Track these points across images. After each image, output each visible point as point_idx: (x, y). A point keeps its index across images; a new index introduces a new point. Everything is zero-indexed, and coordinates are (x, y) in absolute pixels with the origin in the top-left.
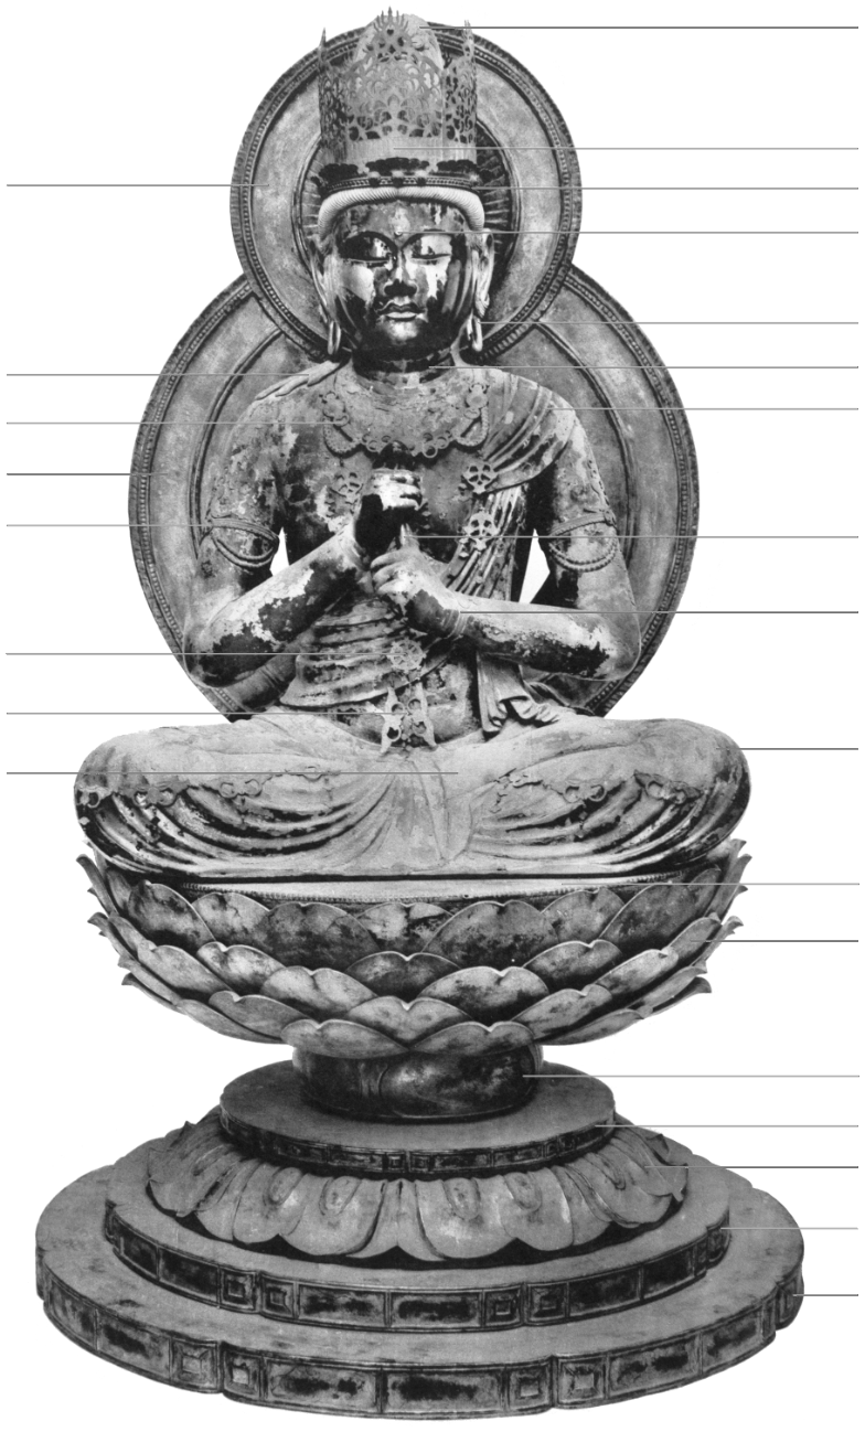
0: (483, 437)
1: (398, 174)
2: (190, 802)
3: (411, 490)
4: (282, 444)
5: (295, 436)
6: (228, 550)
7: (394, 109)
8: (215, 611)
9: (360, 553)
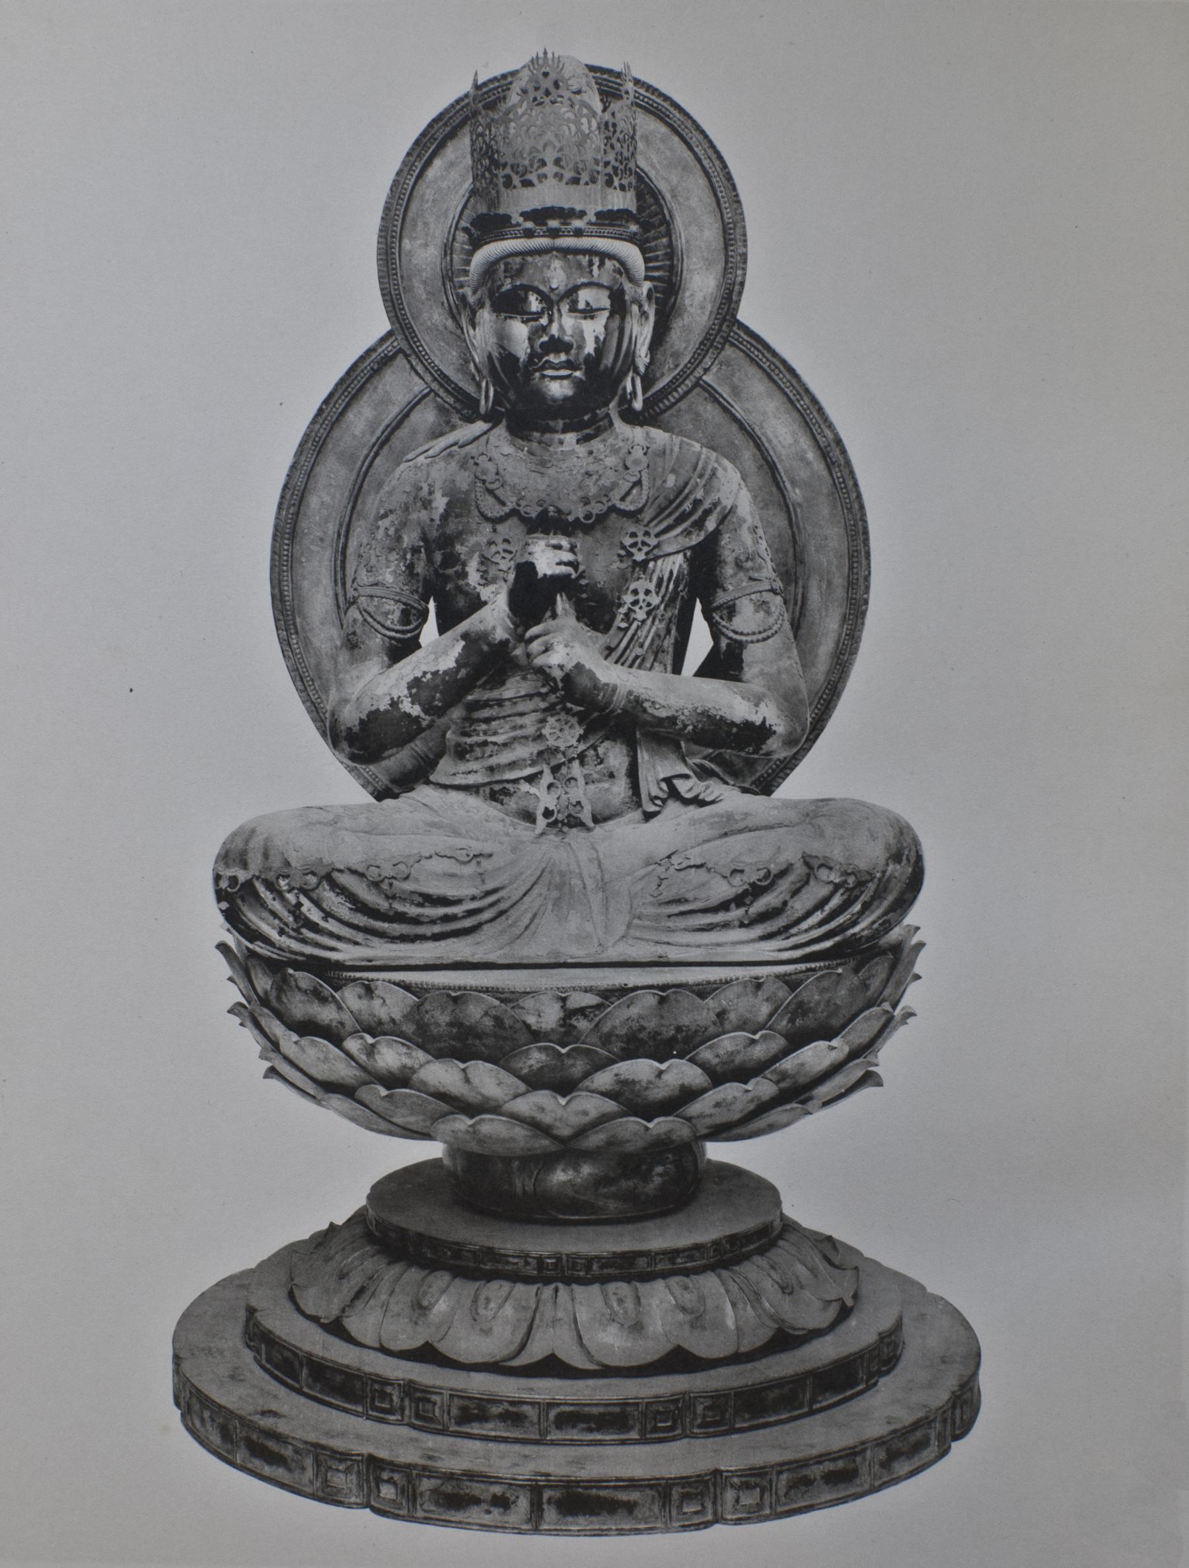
1: (553, 223)
2: (335, 886)
3: (567, 556)
5: (445, 500)
7: (550, 156)
8: (360, 685)
9: (514, 623)
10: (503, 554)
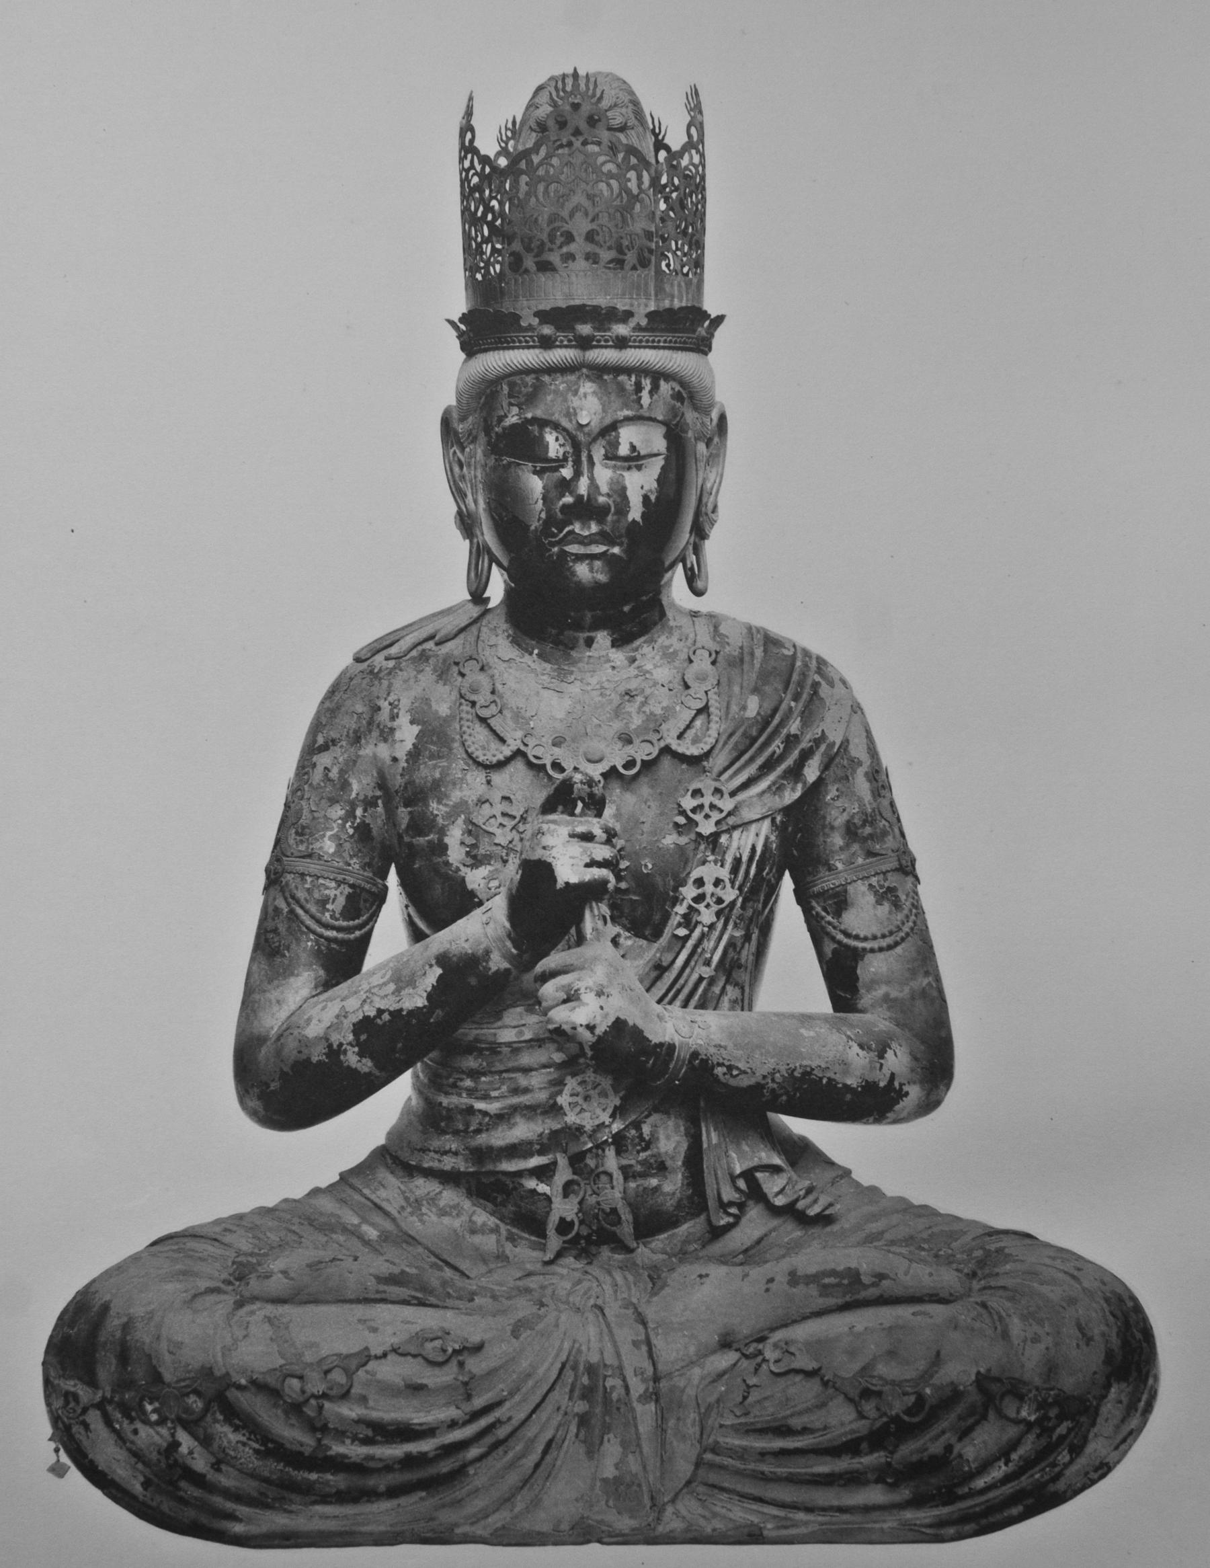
0: (712, 740)
1: (585, 329)
2: (233, 1415)
3: (602, 852)
4: (394, 741)
5: (416, 729)
6: (306, 911)
7: (581, 226)
8: (283, 1014)
10: (500, 820)
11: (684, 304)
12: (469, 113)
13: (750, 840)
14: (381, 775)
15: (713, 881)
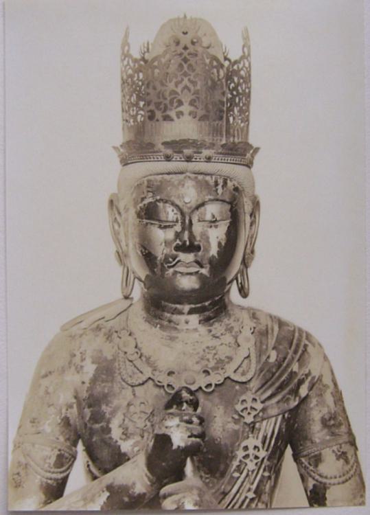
0: (253, 373)
1: (187, 152)
5: (94, 367)
9: (150, 480)
11: (240, 140)
12: (126, 36)
13: (270, 427)
14: (76, 392)
15: (253, 447)
